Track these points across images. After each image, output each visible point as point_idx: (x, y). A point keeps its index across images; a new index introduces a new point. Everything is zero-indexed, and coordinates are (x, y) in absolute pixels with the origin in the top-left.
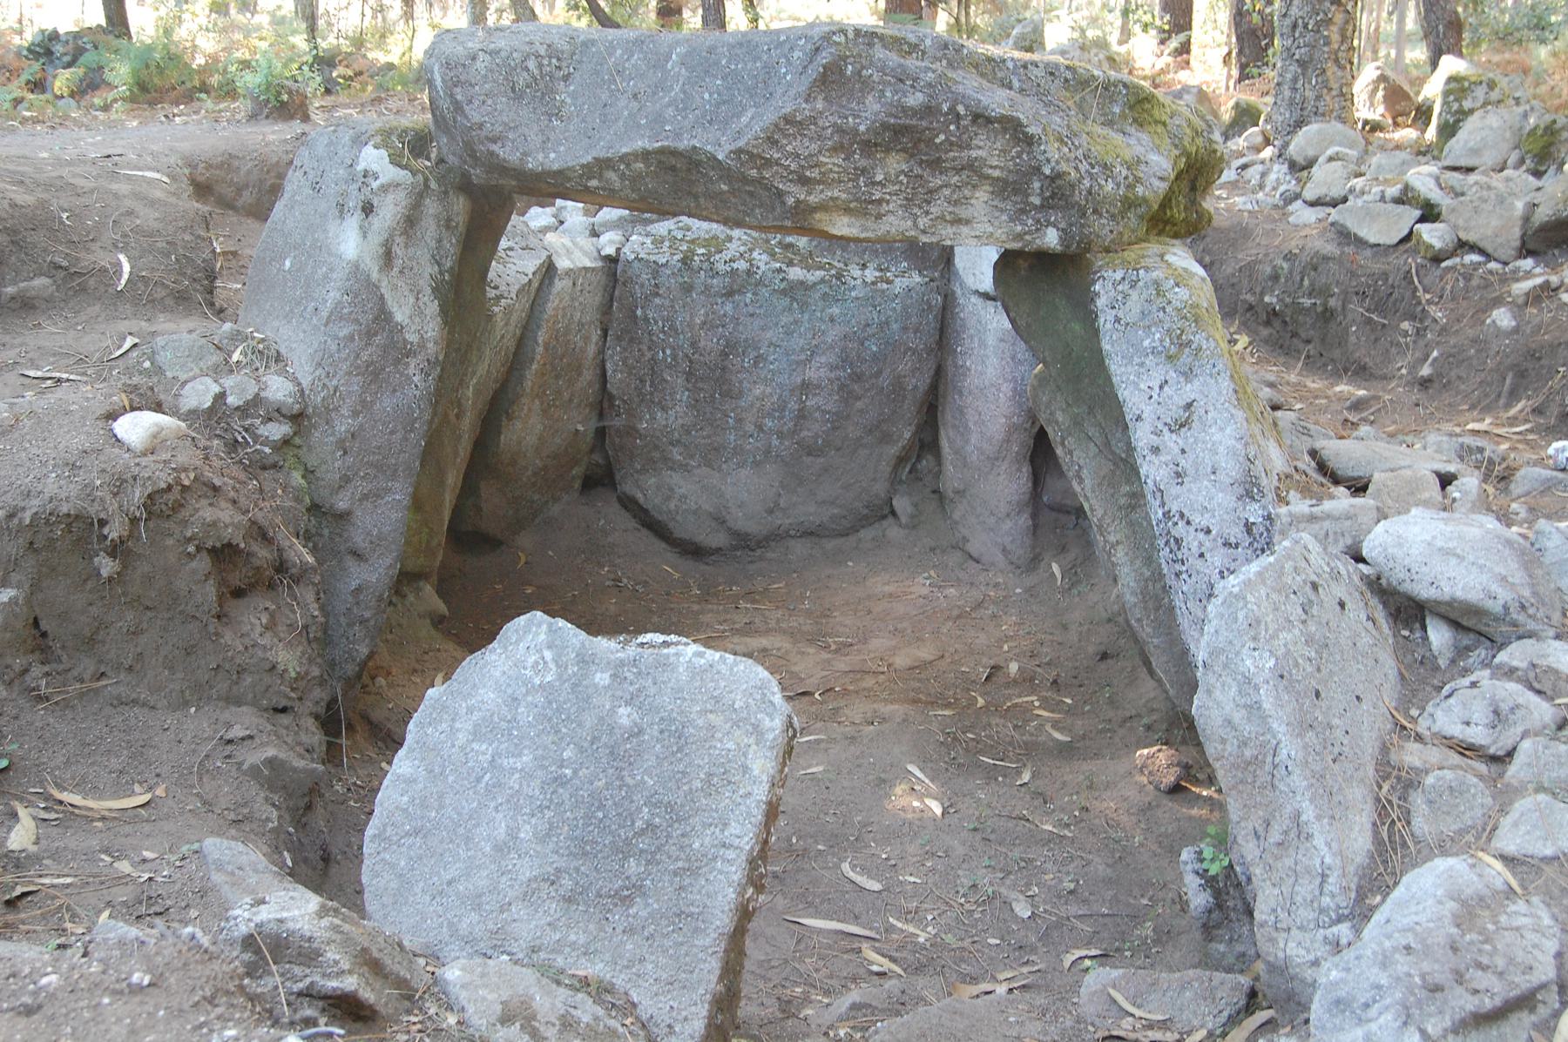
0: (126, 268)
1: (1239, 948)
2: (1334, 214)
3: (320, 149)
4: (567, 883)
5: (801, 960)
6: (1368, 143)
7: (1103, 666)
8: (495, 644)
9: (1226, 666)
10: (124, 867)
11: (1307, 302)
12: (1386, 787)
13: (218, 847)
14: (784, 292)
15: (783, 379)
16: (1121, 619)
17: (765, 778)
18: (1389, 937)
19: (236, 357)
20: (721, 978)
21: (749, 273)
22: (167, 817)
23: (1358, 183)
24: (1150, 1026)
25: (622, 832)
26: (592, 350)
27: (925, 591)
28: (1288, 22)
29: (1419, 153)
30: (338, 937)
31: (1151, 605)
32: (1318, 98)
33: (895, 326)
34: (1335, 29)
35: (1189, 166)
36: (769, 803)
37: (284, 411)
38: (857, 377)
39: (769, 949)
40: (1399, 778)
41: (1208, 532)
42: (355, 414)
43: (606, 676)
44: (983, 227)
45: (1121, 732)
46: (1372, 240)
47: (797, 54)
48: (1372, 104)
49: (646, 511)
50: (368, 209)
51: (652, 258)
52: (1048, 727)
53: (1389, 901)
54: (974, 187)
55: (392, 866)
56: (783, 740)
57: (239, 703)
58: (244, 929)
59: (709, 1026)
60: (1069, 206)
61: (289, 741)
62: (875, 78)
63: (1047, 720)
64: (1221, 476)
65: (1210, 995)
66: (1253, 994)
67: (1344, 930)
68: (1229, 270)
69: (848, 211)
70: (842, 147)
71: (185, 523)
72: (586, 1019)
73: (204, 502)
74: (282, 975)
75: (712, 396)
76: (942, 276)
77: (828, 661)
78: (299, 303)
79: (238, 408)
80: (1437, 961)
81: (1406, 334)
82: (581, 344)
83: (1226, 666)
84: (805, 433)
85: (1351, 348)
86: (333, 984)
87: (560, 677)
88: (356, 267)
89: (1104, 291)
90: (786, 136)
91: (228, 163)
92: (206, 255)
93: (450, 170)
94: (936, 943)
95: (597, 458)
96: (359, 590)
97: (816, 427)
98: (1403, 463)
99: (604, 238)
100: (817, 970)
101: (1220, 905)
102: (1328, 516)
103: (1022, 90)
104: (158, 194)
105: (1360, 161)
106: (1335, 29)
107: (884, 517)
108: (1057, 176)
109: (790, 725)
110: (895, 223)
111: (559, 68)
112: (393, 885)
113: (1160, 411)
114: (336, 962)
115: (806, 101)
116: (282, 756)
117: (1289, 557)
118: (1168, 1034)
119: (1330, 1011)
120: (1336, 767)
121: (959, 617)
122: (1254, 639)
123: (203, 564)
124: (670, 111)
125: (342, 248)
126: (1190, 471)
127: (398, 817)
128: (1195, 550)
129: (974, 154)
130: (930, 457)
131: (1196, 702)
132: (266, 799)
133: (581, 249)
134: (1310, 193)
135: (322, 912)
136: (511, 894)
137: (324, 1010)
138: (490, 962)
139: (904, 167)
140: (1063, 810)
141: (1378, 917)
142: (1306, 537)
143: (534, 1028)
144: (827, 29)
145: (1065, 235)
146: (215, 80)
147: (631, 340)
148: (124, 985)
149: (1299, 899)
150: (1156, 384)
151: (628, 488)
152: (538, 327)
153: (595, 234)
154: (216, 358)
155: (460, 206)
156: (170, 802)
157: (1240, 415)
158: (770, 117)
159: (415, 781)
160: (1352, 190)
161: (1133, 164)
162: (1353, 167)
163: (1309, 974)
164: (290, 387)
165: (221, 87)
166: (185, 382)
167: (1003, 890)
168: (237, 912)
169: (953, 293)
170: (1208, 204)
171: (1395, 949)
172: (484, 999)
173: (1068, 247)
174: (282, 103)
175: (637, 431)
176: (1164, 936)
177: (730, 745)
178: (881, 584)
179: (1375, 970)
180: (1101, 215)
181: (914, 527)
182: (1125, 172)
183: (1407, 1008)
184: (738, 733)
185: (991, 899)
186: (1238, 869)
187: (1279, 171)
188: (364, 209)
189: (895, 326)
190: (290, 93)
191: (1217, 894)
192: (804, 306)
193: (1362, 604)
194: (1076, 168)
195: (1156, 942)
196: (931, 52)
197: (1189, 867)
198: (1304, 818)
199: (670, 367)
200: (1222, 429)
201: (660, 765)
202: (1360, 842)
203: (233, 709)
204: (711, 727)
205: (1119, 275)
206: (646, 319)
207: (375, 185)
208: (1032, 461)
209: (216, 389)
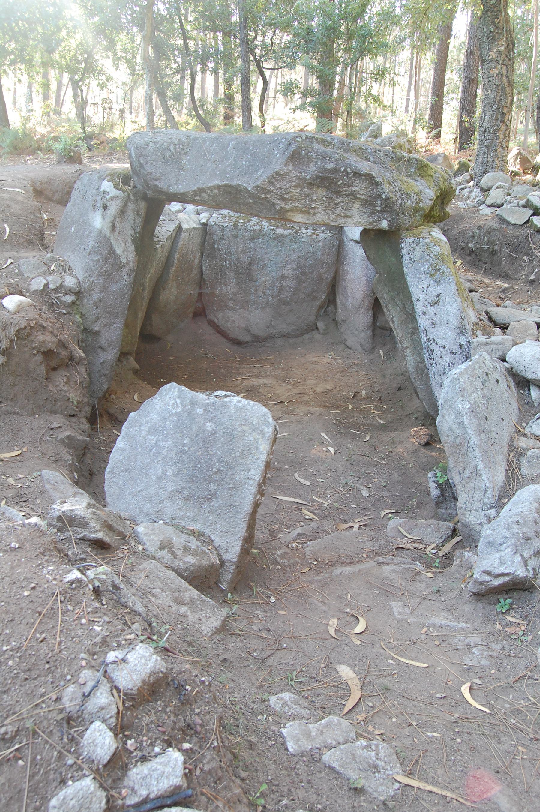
0: (8, 230)
1: (450, 511)
2: (499, 211)
3: (85, 182)
4: (186, 493)
5: (278, 514)
6: (513, 181)
7: (399, 393)
8: (157, 396)
9: (450, 407)
10: (11, 481)
11: (486, 247)
12: (512, 455)
13: (46, 473)
14: (275, 239)
15: (273, 274)
16: (407, 374)
17: (265, 452)
18: (511, 518)
19: (53, 268)
20: (247, 531)
21: (260, 231)
22: (28, 460)
23: (509, 198)
24: (414, 542)
25: (208, 473)
26: (197, 261)
27: (329, 360)
28: (482, 129)
29: (534, 186)
30: (95, 517)
31: (420, 372)
32: (493, 161)
33: (319, 253)
34: (501, 133)
35: (441, 193)
36: (267, 462)
37: (73, 291)
38: (303, 274)
39: (266, 509)
40: (517, 452)
41: (444, 347)
42: (101, 292)
43: (202, 410)
44: (357, 219)
45: (406, 420)
46: (513, 222)
47: (281, 146)
48: (515, 164)
49: (218, 326)
50: (105, 207)
51: (222, 224)
52: (377, 418)
53: (511, 502)
54: (354, 202)
55: (117, 484)
56: (272, 436)
57: (56, 414)
58: (58, 514)
59: (242, 549)
60: (393, 211)
61: (76, 427)
62: (314, 156)
63: (377, 414)
64: (450, 325)
65: (438, 530)
66: (454, 530)
67: (492, 512)
68: (455, 233)
69: (301, 212)
70: (299, 185)
71: (32, 341)
72: (193, 547)
73: (39, 333)
74: (73, 531)
75: (245, 280)
76: (339, 233)
77: (290, 389)
78: (78, 246)
79: (53, 289)
80: (529, 528)
81: (525, 262)
82: (192, 259)
83: (450, 407)
84: (282, 296)
85: (503, 266)
86: (93, 535)
87: (183, 410)
88: (100, 231)
89: (405, 247)
90: (277, 181)
91: (49, 181)
92: (40, 224)
93: (139, 191)
94: (331, 507)
95: (199, 305)
96: (103, 363)
97: (286, 294)
98: (523, 318)
99: (202, 215)
100: (284, 518)
101: (443, 495)
102: (493, 343)
103: (374, 162)
104: (20, 198)
105: (509, 188)
106: (501, 133)
107: (313, 330)
108: (387, 199)
109: (276, 429)
110: (321, 217)
111: (183, 149)
112: (117, 491)
113: (427, 297)
114: (94, 527)
115: (285, 166)
116: (73, 434)
117: (477, 362)
118: (421, 545)
119: (486, 546)
120: (493, 447)
121: (343, 371)
122: (462, 396)
123: (40, 358)
124: (229, 169)
125: (95, 223)
126: (438, 323)
127: (119, 464)
128: (439, 355)
129: (354, 189)
130: (332, 306)
131: (438, 420)
132: (67, 452)
133: (193, 220)
134: (488, 202)
135: (89, 506)
136: (164, 496)
137: (90, 545)
138: (156, 524)
139: (325, 194)
140: (382, 452)
141: (506, 508)
142: (485, 354)
143: (173, 551)
144: (294, 135)
145: (390, 223)
146: (44, 145)
147: (213, 258)
148: (8, 547)
149: (475, 499)
150: (425, 286)
151: (211, 317)
152: (175, 252)
153: (198, 214)
154: (45, 268)
155: (143, 205)
156: (29, 454)
157: (459, 300)
158: (270, 173)
159: (125, 450)
160: (506, 201)
161: (419, 194)
162: (506, 191)
163: (478, 528)
164: (74, 281)
165: (46, 148)
166: (32, 279)
167: (358, 485)
168: (55, 506)
169: (343, 240)
170: (448, 209)
171: (513, 522)
172: (153, 540)
173: (391, 228)
174: (71, 156)
175: (215, 294)
176: (420, 505)
177: (252, 439)
178: (312, 358)
179: (505, 531)
180: (405, 215)
181: (325, 334)
182: (415, 197)
183: (517, 547)
184: (254, 434)
185: (353, 489)
186: (451, 481)
187: (476, 191)
188: (103, 207)
189: (319, 253)
190: (74, 152)
191: (442, 490)
192: (282, 244)
193: (505, 380)
194: (396, 195)
195: (417, 507)
196: (337, 145)
197: (431, 479)
198: (479, 468)
199: (228, 268)
200: (451, 306)
201: (223, 446)
202: (501, 477)
203: (53, 415)
204: (244, 431)
205: (412, 240)
206: (219, 249)
207: (108, 197)
208: (373, 309)
209: (45, 282)
